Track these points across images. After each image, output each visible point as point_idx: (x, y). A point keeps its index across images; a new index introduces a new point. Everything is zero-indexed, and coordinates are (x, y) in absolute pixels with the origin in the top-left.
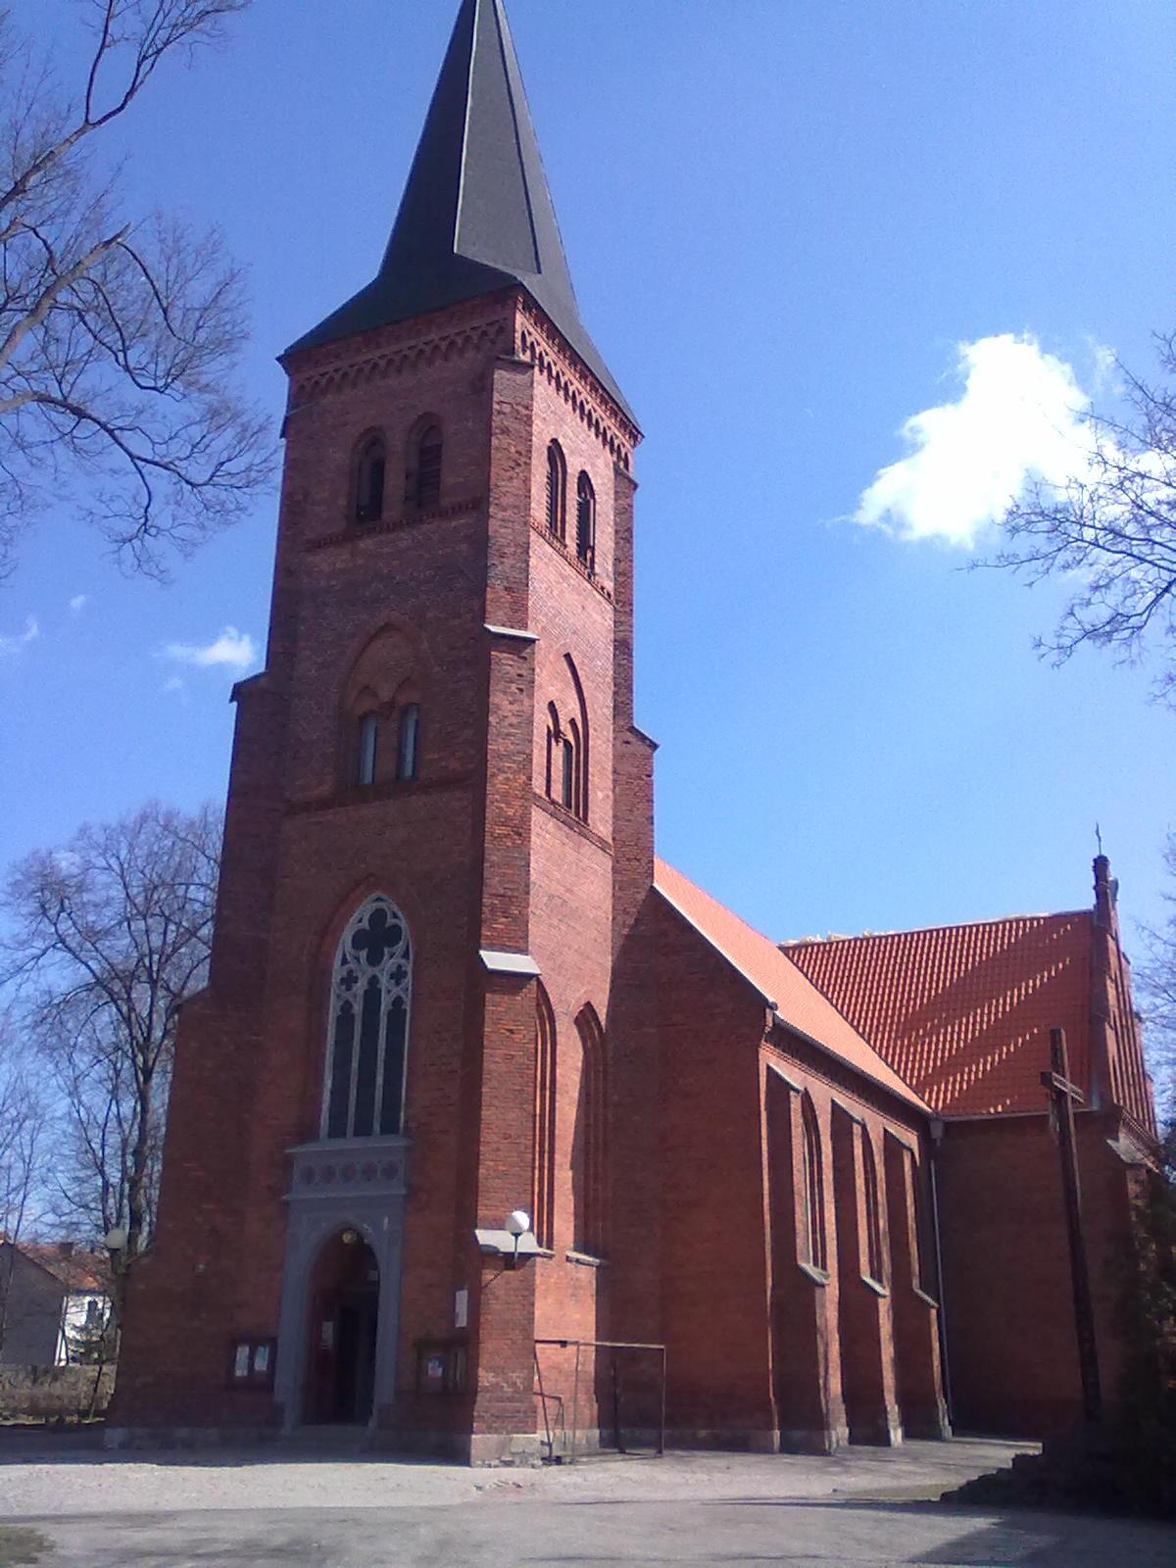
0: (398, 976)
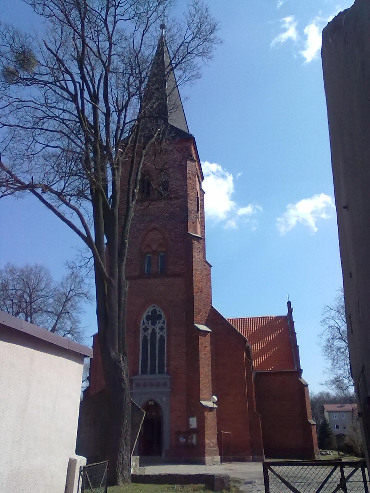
0: (162, 329)
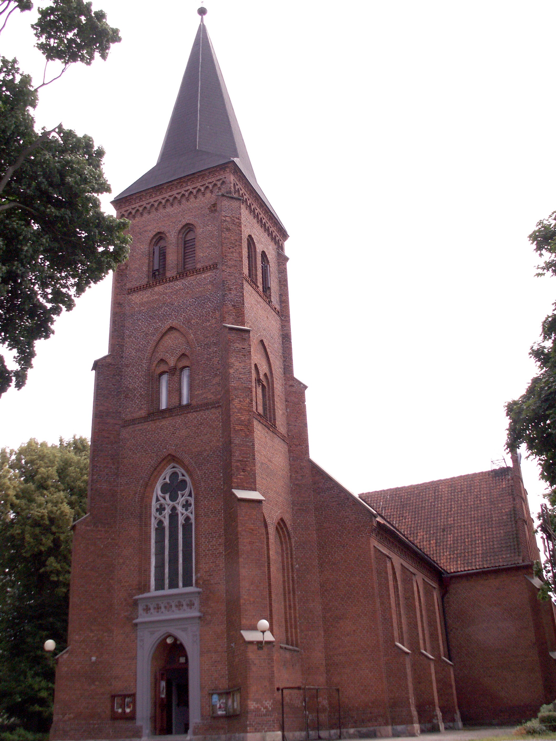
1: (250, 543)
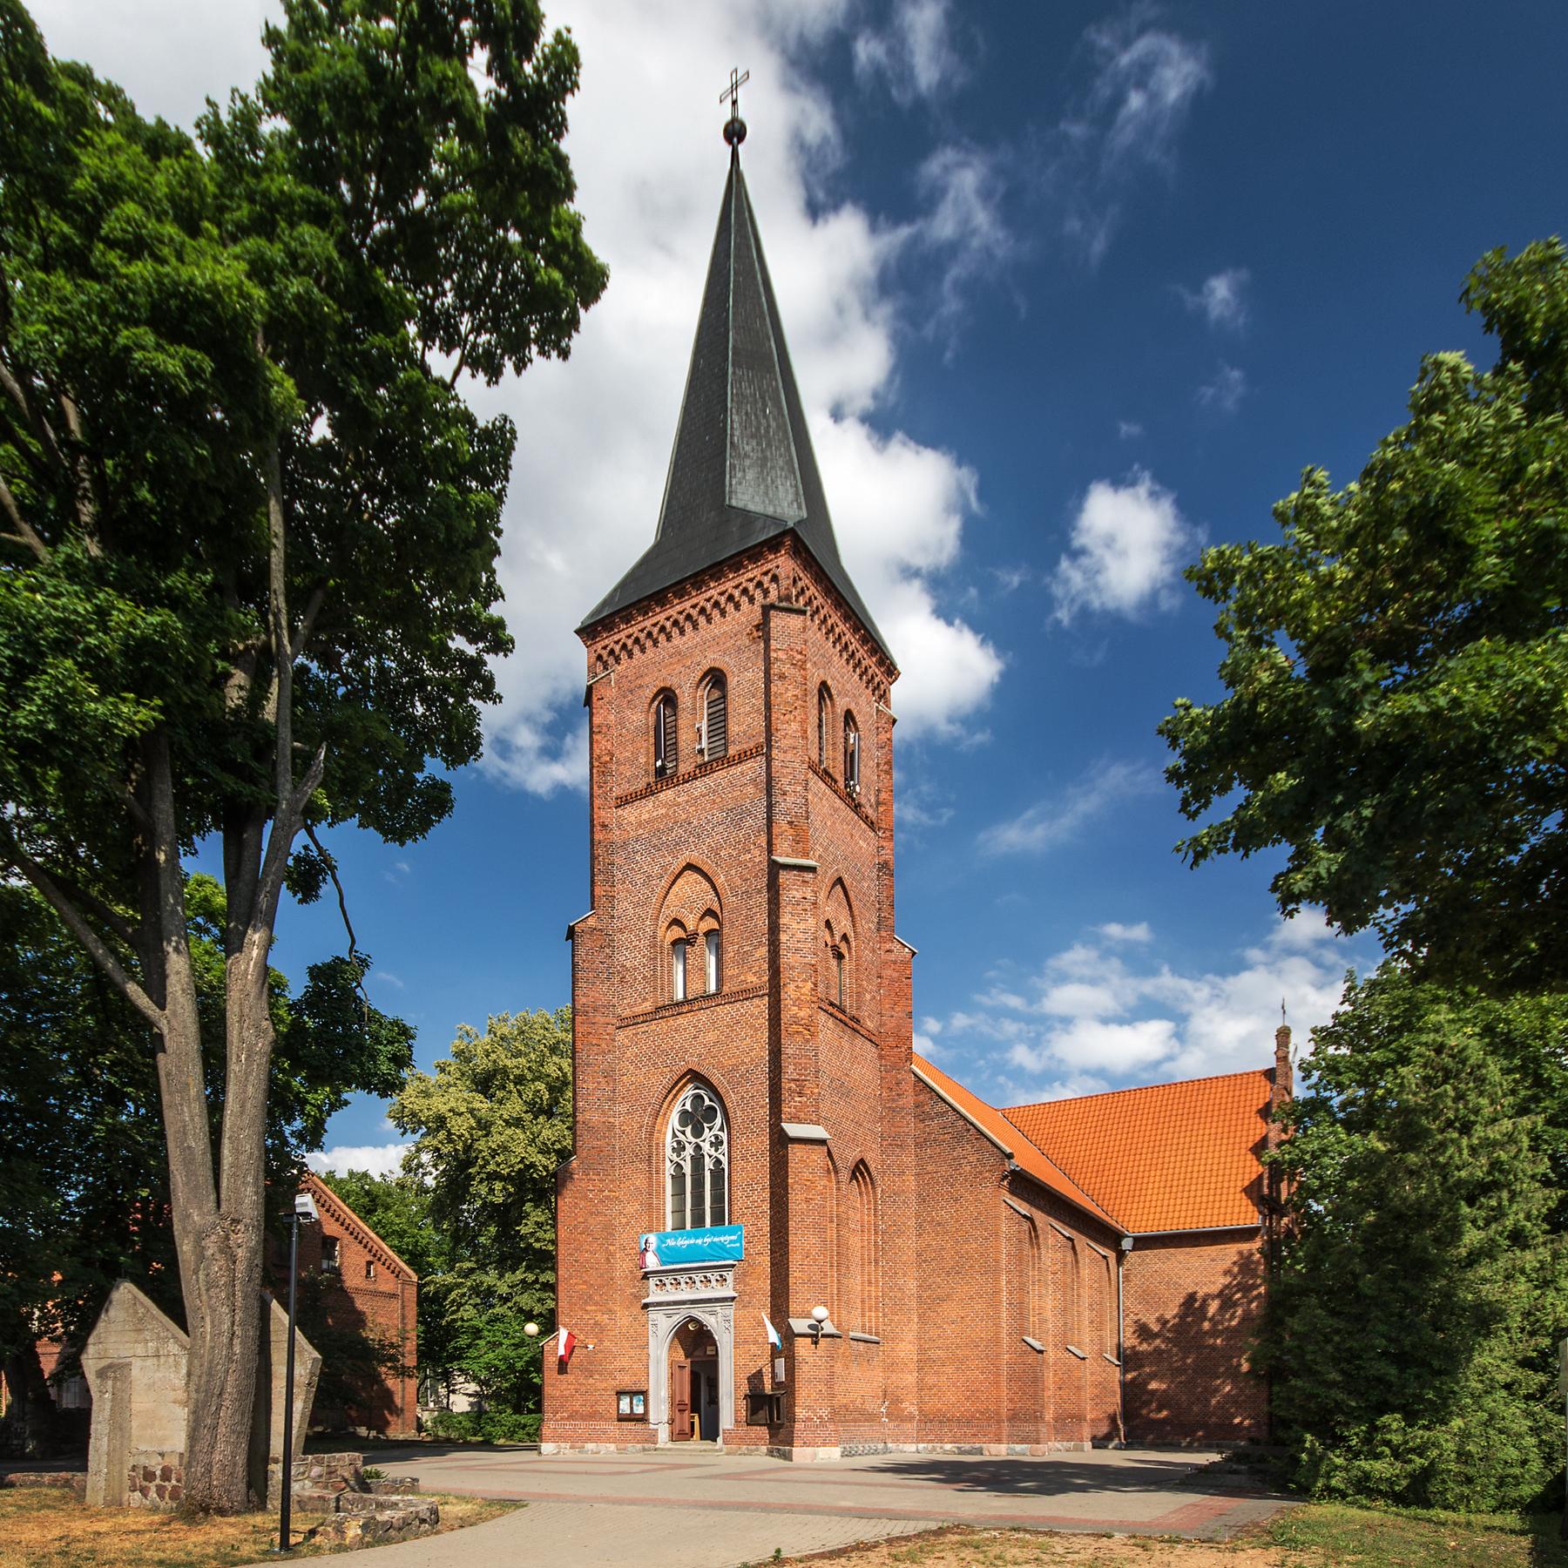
0: (717, 1143)
1: (807, 1201)
